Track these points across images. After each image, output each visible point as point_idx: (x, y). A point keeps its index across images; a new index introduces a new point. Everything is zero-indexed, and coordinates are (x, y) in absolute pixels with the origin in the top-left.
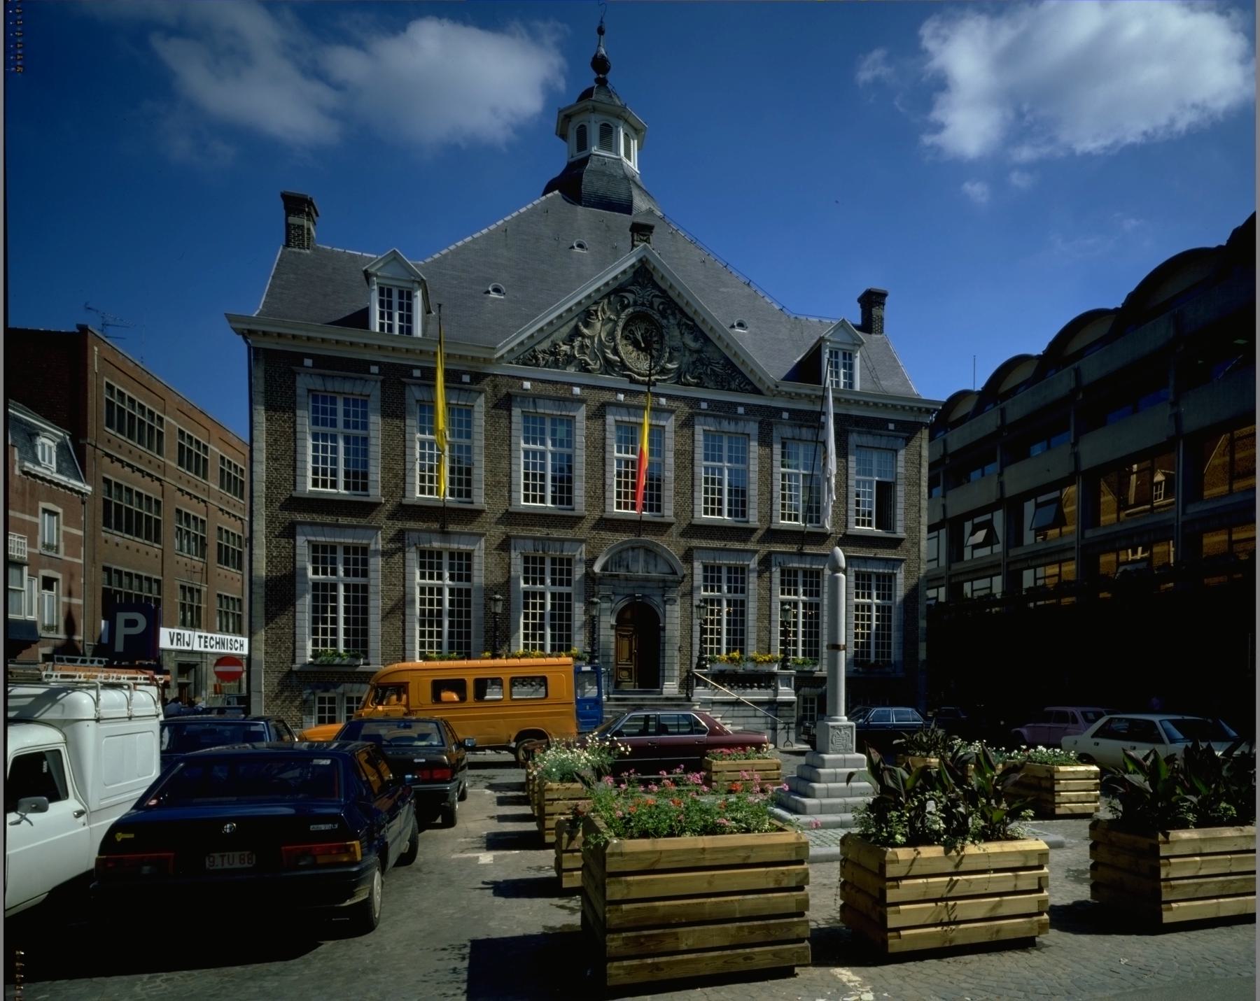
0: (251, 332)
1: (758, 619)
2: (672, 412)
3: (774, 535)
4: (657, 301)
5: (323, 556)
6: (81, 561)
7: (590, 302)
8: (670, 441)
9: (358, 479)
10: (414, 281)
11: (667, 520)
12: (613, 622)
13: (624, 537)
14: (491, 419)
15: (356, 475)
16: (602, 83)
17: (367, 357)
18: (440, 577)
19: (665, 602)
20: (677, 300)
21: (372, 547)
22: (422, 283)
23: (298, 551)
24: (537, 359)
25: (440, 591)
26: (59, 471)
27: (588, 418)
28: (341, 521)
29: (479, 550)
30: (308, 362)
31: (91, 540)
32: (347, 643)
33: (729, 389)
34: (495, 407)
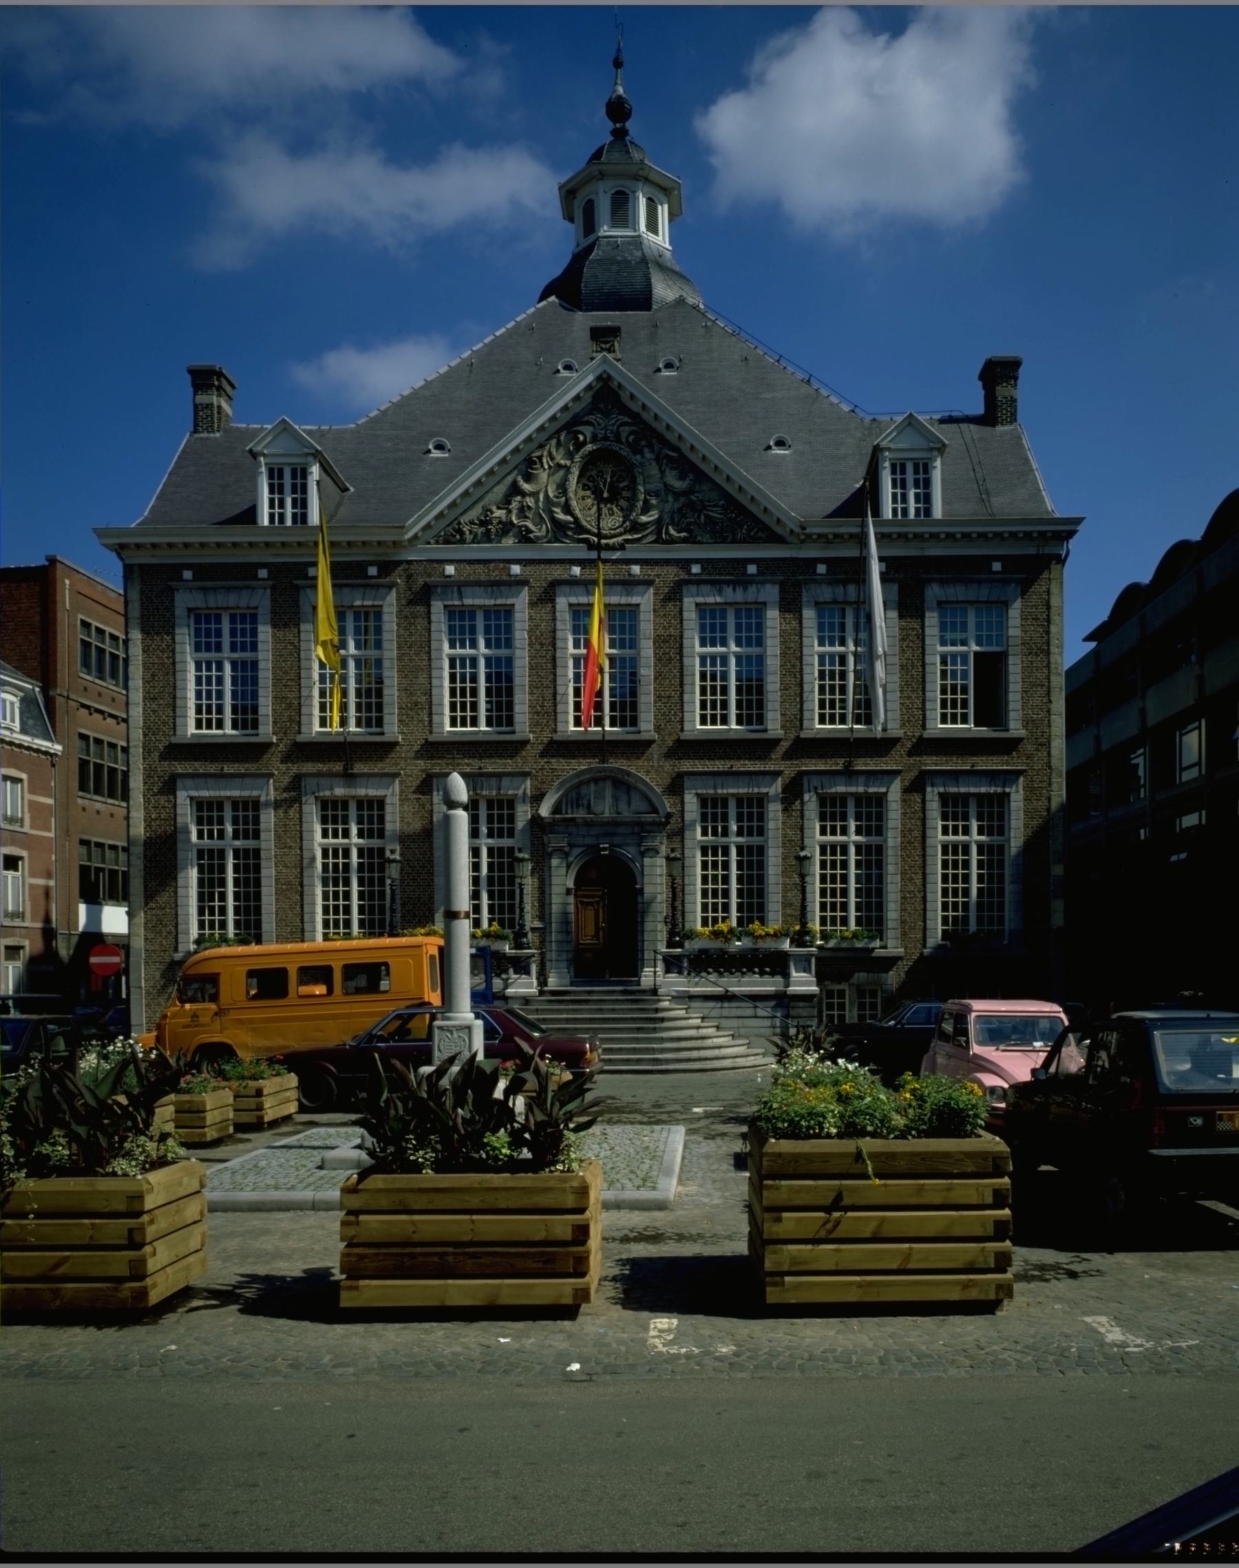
0: (123, 547)
1: (785, 873)
2: (649, 583)
3: (805, 747)
4: (625, 430)
5: (207, 811)
6: (52, 835)
7: (534, 445)
8: (647, 625)
9: (246, 715)
10: (307, 455)
11: (771, 735)
12: (570, 884)
13: (582, 765)
14: (405, 620)
15: (245, 710)
16: (620, 135)
17: (255, 559)
18: (346, 834)
19: (642, 855)
20: (655, 425)
21: (263, 799)
22: (317, 455)
23: (179, 811)
24: (461, 533)
25: (346, 853)
26: (24, 731)
27: (532, 604)
28: (226, 770)
29: (392, 794)
30: (188, 575)
31: (64, 807)
32: (237, 924)
33: (734, 541)
34: (411, 603)
